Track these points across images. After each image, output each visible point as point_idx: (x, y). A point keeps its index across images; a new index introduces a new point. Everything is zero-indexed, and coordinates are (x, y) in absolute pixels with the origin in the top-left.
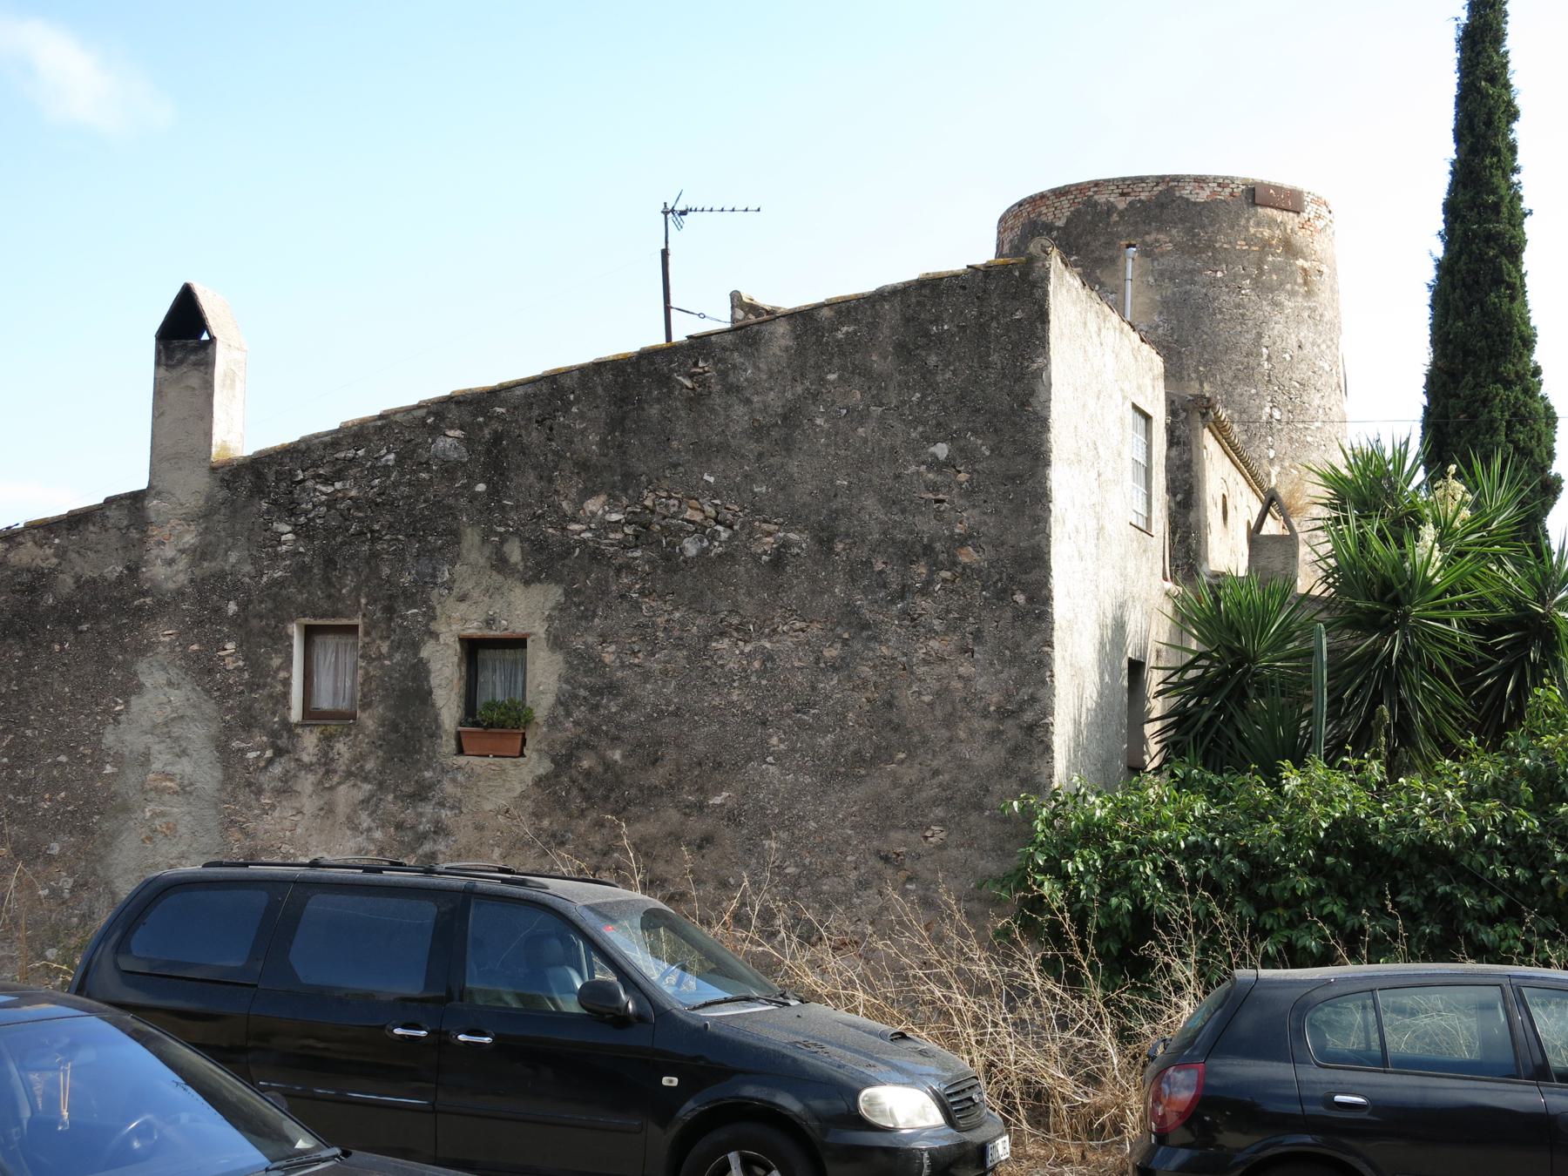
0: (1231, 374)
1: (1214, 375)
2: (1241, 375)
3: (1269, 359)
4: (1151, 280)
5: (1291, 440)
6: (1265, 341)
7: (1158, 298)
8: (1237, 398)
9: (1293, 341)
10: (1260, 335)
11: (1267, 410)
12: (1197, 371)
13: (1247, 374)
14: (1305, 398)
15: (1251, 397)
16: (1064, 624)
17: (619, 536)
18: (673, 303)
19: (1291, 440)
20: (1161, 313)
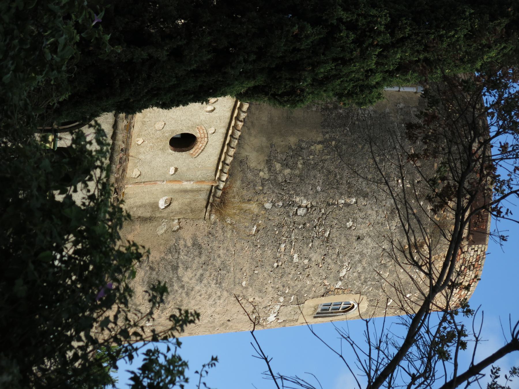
0: (332, 168)
1: (329, 153)
2: (331, 177)
3: (347, 205)
4: (402, 105)
5: (280, 226)
6: (362, 202)
7: (387, 110)
8: (312, 173)
9: (363, 230)
10: (365, 196)
11: (305, 203)
12: (332, 139)
13: (332, 184)
14: (317, 243)
15: (314, 186)
16: (188, 130)
17: (296, 256)
18: (453, 365)
19: (280, 226)
20: (375, 112)
